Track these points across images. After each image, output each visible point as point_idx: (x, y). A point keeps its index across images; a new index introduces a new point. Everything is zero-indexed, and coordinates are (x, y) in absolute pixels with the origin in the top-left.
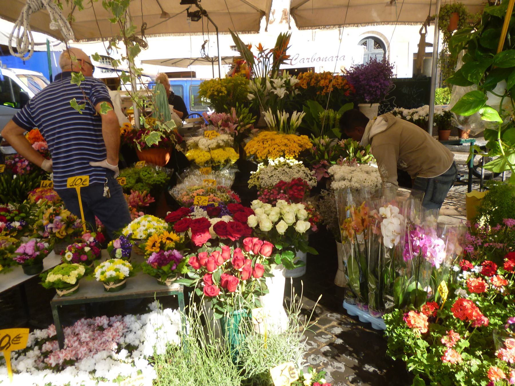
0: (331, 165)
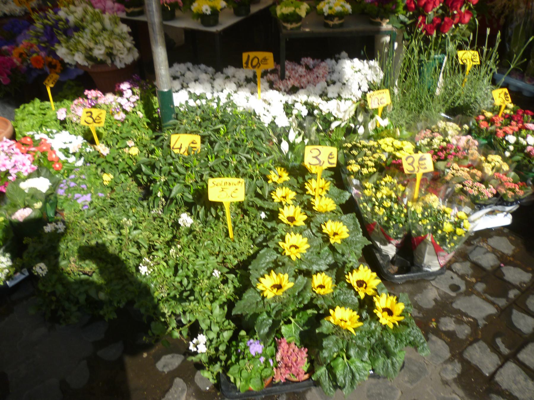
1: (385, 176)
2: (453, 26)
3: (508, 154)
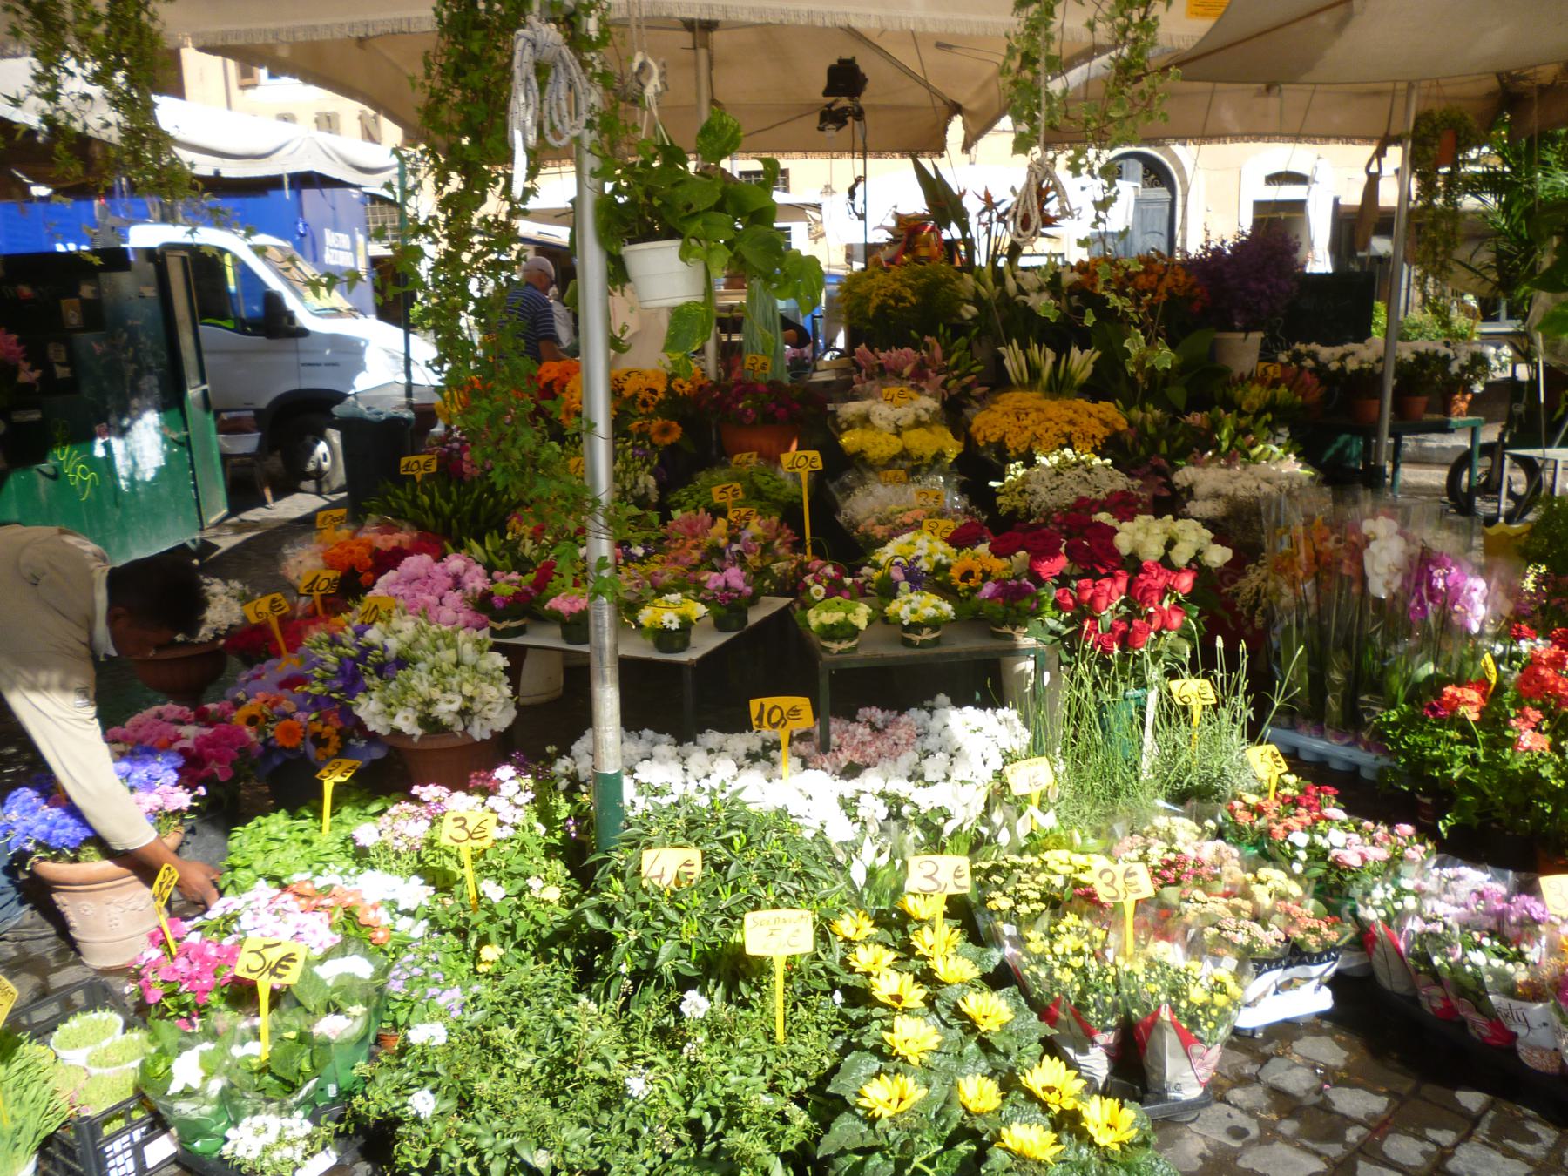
0: (1179, 468)
1: (1065, 915)
2: (1152, 635)
3: (1298, 868)
